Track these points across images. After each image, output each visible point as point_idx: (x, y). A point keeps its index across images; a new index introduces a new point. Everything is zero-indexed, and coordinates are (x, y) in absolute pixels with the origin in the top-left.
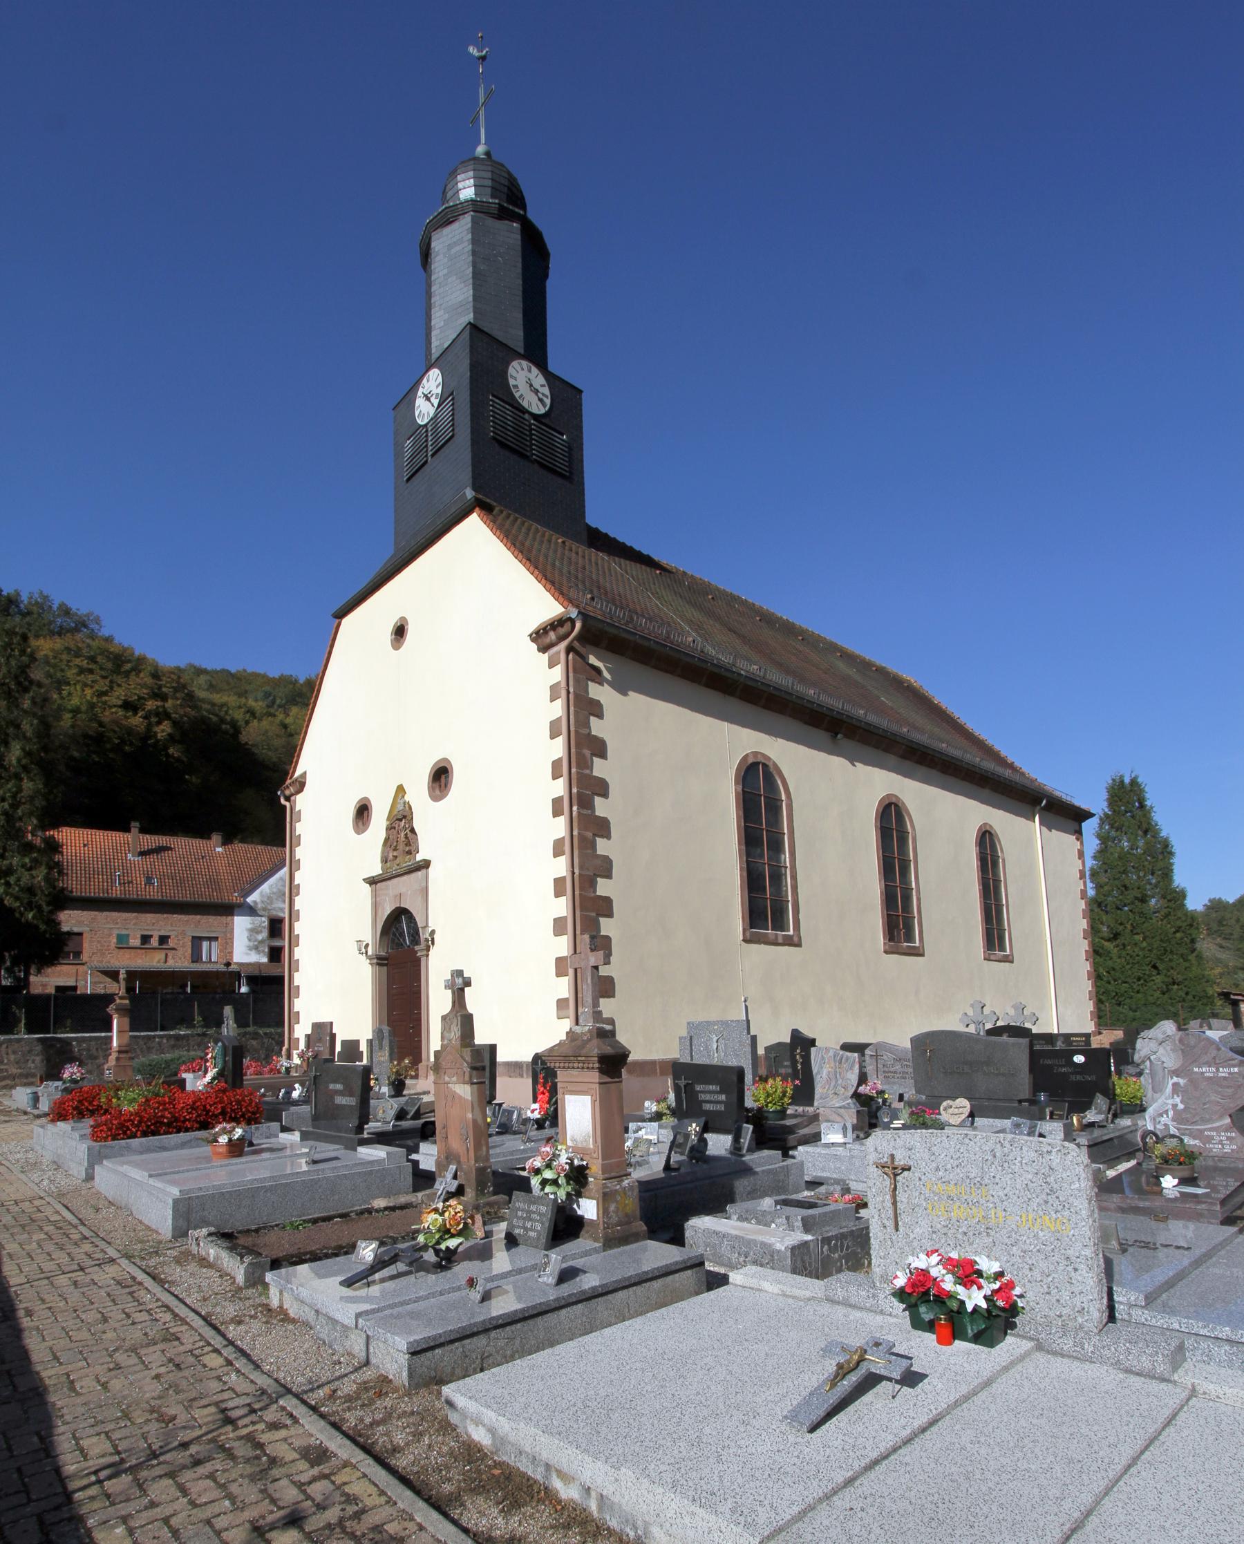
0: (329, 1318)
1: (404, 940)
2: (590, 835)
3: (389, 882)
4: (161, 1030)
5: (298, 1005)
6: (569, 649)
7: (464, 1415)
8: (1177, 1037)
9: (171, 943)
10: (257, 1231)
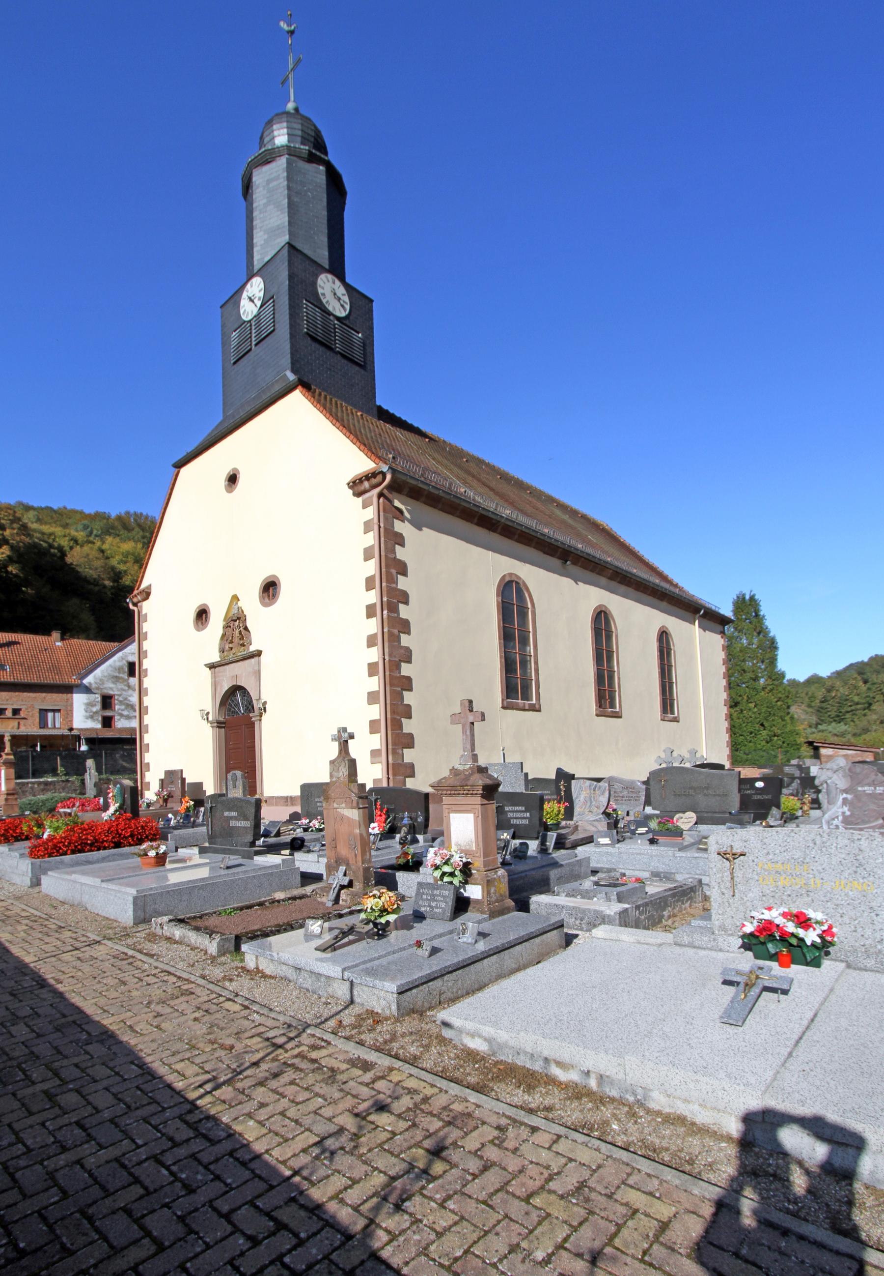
0: (312, 972)
1: (239, 709)
2: (396, 631)
3: (226, 667)
4: (34, 776)
5: (148, 758)
6: (381, 495)
7: (460, 1031)
8: (847, 768)
9: (22, 714)
10: (201, 917)
